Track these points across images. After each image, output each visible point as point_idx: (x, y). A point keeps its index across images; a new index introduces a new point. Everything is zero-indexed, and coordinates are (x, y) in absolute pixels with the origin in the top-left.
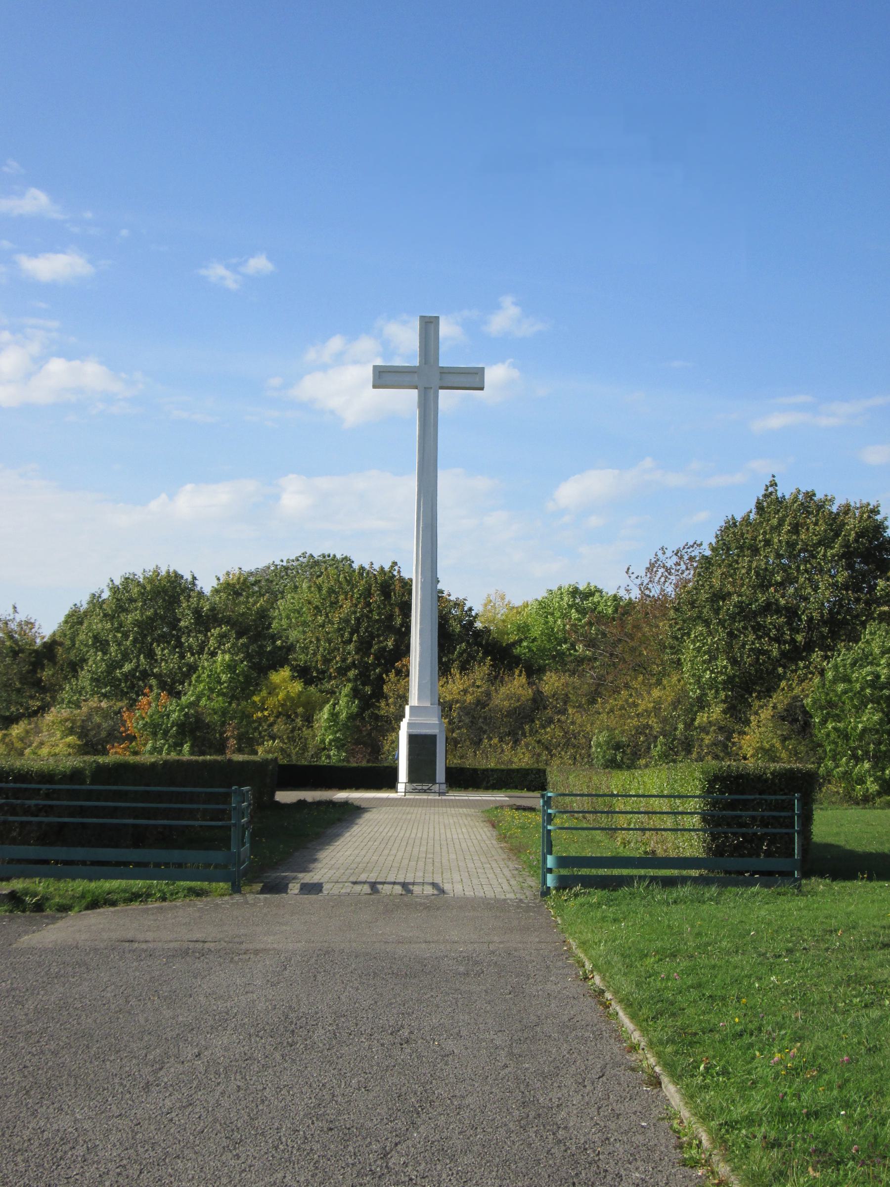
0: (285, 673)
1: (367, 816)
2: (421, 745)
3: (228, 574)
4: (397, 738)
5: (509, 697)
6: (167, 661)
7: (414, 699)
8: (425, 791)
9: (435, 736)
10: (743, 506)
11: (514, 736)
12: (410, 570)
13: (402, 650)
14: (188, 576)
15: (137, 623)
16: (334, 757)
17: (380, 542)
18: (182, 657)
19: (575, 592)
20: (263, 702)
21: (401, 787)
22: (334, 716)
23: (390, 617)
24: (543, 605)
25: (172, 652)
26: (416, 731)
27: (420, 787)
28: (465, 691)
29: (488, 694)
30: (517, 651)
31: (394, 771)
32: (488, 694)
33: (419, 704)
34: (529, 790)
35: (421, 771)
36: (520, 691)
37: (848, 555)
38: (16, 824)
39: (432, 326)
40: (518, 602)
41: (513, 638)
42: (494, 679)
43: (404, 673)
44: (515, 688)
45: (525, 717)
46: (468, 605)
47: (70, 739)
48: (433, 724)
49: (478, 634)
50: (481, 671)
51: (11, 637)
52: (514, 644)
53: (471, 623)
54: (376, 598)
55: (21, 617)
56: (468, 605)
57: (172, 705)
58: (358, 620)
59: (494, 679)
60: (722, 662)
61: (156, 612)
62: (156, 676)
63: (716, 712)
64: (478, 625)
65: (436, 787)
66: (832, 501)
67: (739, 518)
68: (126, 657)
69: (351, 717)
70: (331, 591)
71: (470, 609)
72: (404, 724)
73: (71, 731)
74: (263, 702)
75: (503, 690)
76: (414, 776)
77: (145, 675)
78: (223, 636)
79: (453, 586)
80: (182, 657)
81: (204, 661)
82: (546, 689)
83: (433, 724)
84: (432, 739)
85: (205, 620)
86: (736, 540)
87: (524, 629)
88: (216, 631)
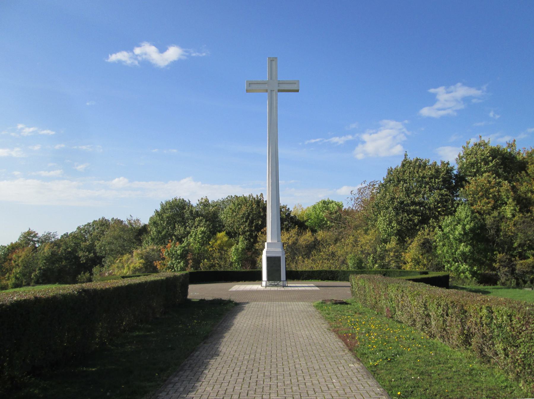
0: (223, 233)
1: (242, 309)
2: (273, 262)
3: (202, 199)
4: (261, 259)
5: (305, 240)
6: (180, 230)
7: (269, 239)
8: (276, 286)
9: (280, 257)
10: (397, 164)
11: (308, 255)
12: (267, 198)
13: (264, 224)
14: (187, 201)
15: (167, 217)
16: (237, 268)
17: (256, 187)
18: (185, 228)
19: (324, 202)
20: (213, 244)
21: (264, 283)
22: (237, 250)
23: (260, 212)
24: (314, 207)
25: (182, 226)
26: (270, 255)
27: (273, 283)
28: (288, 239)
29: (297, 240)
30: (306, 224)
31: (260, 274)
32: (297, 240)
33: (272, 243)
34: (322, 280)
35: (274, 276)
36: (309, 238)
37: (445, 181)
38: (261, 247)
39: (274, 63)
40: (305, 207)
41: (305, 219)
42: (299, 234)
43: (265, 233)
44: (307, 237)
45: (313, 247)
46: (288, 207)
47: (141, 261)
48: (278, 252)
49: (292, 218)
50: (294, 231)
51: (132, 226)
52: (306, 221)
53: (289, 214)
54: (255, 206)
55: (134, 218)
56: (288, 207)
57: (178, 246)
58: (248, 213)
59: (299, 234)
60: (394, 224)
61: (176, 214)
62: (175, 236)
63: (393, 244)
64: (292, 215)
65: (281, 283)
66: (429, 162)
67: (393, 168)
68: (164, 228)
69: (243, 250)
70: (238, 204)
71: (289, 209)
72: (264, 252)
73: (142, 258)
74: (213, 244)
75: (302, 238)
76: (269, 279)
77: (171, 235)
78: (201, 221)
79: (283, 202)
80: (185, 228)
81: (193, 230)
82: (319, 238)
83: (278, 252)
84: (279, 259)
85: (195, 215)
86: (395, 178)
87: (309, 216)
88: (197, 219)
